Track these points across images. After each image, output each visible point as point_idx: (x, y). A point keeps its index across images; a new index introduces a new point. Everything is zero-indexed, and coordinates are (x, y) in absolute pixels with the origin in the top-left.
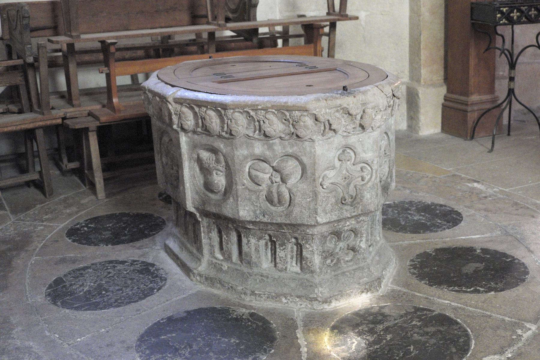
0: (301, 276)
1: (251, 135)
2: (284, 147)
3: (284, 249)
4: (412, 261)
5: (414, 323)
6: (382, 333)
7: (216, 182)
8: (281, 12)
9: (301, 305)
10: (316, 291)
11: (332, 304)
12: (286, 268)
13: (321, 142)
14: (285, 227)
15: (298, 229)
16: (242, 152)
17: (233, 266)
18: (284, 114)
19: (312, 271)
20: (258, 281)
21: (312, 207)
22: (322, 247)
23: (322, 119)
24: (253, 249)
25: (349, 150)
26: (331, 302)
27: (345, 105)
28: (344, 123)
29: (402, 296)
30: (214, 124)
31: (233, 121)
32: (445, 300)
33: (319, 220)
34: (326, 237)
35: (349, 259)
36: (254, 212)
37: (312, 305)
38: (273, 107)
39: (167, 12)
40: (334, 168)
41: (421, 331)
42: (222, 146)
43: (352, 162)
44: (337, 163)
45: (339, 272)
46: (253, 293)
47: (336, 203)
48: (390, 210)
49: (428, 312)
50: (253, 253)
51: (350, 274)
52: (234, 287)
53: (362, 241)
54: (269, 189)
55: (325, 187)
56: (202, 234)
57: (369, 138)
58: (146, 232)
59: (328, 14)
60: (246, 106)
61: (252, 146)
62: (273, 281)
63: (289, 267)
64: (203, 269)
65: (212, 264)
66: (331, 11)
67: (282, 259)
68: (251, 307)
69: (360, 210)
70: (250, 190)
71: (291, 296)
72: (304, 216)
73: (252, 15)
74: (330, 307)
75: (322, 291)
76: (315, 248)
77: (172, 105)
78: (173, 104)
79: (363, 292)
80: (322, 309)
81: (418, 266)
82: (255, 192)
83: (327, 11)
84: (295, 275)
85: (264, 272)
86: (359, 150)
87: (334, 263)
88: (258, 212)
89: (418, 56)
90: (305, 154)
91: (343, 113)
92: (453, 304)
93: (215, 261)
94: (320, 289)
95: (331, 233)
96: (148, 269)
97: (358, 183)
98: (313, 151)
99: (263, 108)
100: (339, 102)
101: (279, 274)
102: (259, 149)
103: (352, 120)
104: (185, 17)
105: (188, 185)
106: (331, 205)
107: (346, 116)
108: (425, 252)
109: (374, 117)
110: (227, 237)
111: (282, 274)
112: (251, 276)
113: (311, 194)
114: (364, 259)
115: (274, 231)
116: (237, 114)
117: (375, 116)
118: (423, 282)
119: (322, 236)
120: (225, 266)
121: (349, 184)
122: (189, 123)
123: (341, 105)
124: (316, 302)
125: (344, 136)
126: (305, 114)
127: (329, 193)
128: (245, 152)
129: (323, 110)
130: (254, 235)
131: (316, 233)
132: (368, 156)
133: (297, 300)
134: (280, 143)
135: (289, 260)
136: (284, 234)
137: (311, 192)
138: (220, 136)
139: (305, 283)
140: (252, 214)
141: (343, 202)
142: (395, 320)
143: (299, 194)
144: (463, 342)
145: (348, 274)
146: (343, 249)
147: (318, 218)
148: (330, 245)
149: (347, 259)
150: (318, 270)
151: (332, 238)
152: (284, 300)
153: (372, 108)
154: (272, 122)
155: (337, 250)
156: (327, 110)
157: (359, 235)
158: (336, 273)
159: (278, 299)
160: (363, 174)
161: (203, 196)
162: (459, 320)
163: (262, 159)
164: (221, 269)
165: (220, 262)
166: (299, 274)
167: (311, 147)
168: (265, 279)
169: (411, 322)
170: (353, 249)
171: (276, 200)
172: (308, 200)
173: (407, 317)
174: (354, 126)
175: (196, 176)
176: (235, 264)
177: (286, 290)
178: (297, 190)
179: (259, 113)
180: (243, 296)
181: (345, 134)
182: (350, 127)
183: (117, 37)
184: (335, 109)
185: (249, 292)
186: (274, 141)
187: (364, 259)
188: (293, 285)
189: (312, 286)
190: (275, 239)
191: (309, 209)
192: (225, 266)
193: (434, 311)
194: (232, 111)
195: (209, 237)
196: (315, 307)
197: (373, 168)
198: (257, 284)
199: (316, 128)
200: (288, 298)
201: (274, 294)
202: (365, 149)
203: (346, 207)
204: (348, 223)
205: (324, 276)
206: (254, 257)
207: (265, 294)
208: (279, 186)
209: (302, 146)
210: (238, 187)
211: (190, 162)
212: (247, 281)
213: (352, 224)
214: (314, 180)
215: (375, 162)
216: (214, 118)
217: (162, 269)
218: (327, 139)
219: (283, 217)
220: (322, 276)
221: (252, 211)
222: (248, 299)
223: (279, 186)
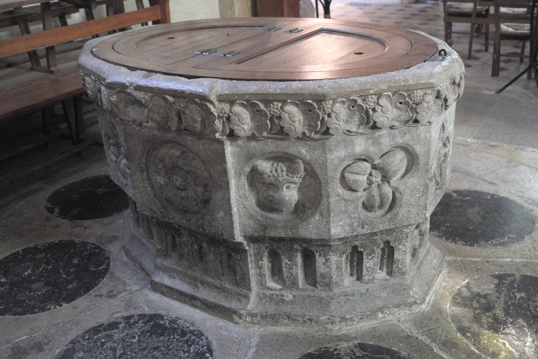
3: (372, 258)
7: (287, 198)
10: (411, 293)
17: (301, 293)
20: (343, 302)
24: (334, 267)
30: (297, 124)
31: (333, 115)
42: (304, 151)
46: (343, 319)
50: (333, 272)
52: (315, 318)
56: (250, 265)
61: (353, 144)
62: (361, 296)
64: (253, 306)
67: (369, 270)
70: (346, 200)
71: (388, 308)
75: (415, 292)
77: (214, 106)
78: (216, 103)
82: (353, 201)
89: (231, 8)
90: (419, 141)
93: (268, 293)
96: (159, 325)
98: (428, 136)
101: (367, 287)
110: (289, 261)
111: (369, 286)
112: (333, 299)
122: (246, 127)
128: (342, 153)
137: (421, 186)
138: (303, 138)
139: (398, 288)
143: (408, 191)
152: (380, 315)
159: (373, 316)
161: (262, 219)
163: (363, 157)
164: (283, 301)
165: (278, 293)
167: (426, 131)
168: (351, 298)
172: (418, 195)
176: (303, 290)
177: (379, 303)
179: (370, 100)
180: (329, 326)
185: (337, 320)
186: (381, 133)
188: (384, 295)
189: (406, 288)
190: (362, 250)
191: (418, 206)
192: (288, 296)
195: (257, 268)
198: (343, 306)
201: (368, 313)
206: (334, 277)
210: (330, 200)
212: (328, 306)
219: (387, 223)
222: (336, 328)
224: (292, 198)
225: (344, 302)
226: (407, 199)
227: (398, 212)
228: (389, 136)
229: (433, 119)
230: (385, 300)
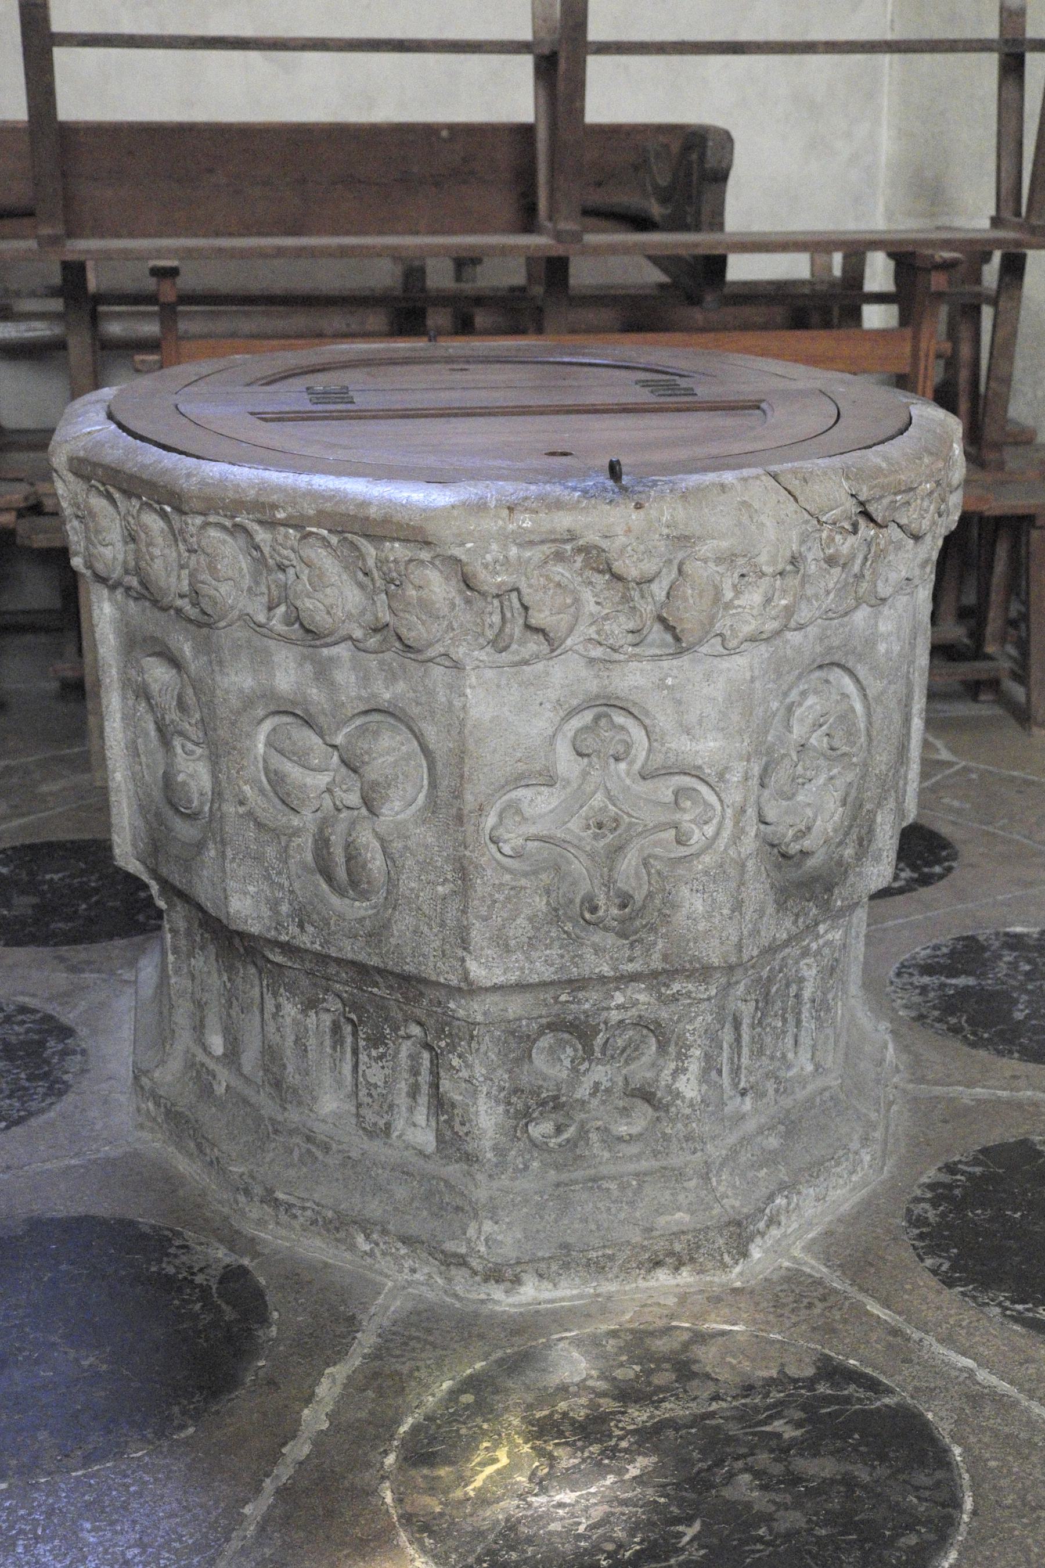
0: (430, 1167)
1: (261, 618)
2: (365, 679)
3: (381, 1057)
4: (951, 1169)
5: (777, 1426)
6: (624, 1444)
7: (181, 778)
8: (890, 216)
9: (413, 1271)
10: (471, 1232)
11: (522, 1290)
12: (388, 1126)
13: (489, 674)
14: (380, 980)
15: (422, 994)
16: (238, 680)
18: (358, 549)
19: (467, 1154)
20: (296, 1154)
21: (451, 915)
22: (510, 1071)
23: (493, 580)
25: (620, 719)
26: (517, 1281)
27: (592, 537)
28: (593, 608)
29: (810, 1306)
32: (964, 1354)
33: (476, 971)
34: (528, 1041)
35: (635, 1130)
36: (274, 905)
37: (449, 1280)
38: (322, 518)
39: (437, 184)
40: (550, 780)
41: (777, 1469)
43: (637, 766)
44: (566, 763)
45: (579, 1174)
46: (269, 1199)
47: (555, 915)
48: (1008, 957)
49: (861, 1394)
50: (288, 1053)
51: (623, 1187)
53: (685, 1070)
54: (321, 830)
55: (507, 849)
57: (708, 677)
58: (141, 918)
59: (996, 222)
60: (239, 505)
62: (343, 1165)
63: (399, 1124)
64: (169, 1078)
65: (193, 1065)
66: (1007, 215)
67: (374, 1092)
68: (251, 1246)
69: (656, 956)
70: (259, 825)
71: (384, 1232)
72: (426, 950)
73: (706, 209)
74: (510, 1300)
75: (494, 1236)
76: (480, 1071)
78: (70, 477)
79: (658, 1264)
80: (482, 1301)
81: (957, 1192)
82: (276, 833)
83: (993, 213)
84: (414, 1159)
85: (319, 1128)
86: (664, 719)
87: (566, 1136)
88: (284, 908)
90: (432, 713)
91: (587, 564)
92: (983, 1376)
93: (201, 1057)
94: (488, 1226)
95: (552, 1027)
97: (658, 851)
98: (457, 703)
99: (290, 517)
100: (564, 521)
102: (287, 674)
103: (626, 599)
104: (502, 203)
105: (118, 776)
106: (530, 919)
107: (600, 580)
108: (1024, 1144)
109: (729, 595)
110: (230, 980)
111: (375, 1147)
113: (448, 868)
114: (688, 1138)
115: (346, 983)
116: (214, 533)
117: (738, 592)
118: (929, 1262)
119: (512, 1033)
120: (223, 1080)
121: (617, 850)
122: (108, 552)
123: (571, 536)
124: (464, 1272)
125: (591, 661)
126: (425, 555)
127: (525, 874)
129: (494, 547)
130: (292, 988)
131: (479, 1018)
132: (707, 748)
133: (403, 1251)
134: (353, 658)
135: (402, 1100)
136: (381, 1006)
140: (266, 913)
141: (587, 916)
142: (716, 1398)
144: (911, 1550)
145: (613, 1186)
146: (607, 1091)
147: (472, 966)
148: (551, 1065)
149: (623, 1129)
150: (489, 1155)
151: (562, 1044)
153: (719, 560)
154: (321, 576)
155: (583, 1091)
156: (514, 551)
157: (672, 1049)
158: (565, 1177)
159: (341, 1235)
160: (677, 816)
162: (957, 1450)
166: (427, 1157)
168: (319, 1154)
169: (770, 1419)
170: (647, 1096)
171: (341, 873)
172: (440, 888)
173: (767, 1395)
174: (631, 626)
175: (141, 748)
176: (247, 1080)
177: (374, 1208)
178: (406, 847)
180: (242, 1198)
181: (597, 652)
182: (618, 628)
183: (189, 254)
184: (547, 549)
185: (258, 1190)
186: (334, 651)
187: (688, 1138)
188: (401, 1193)
189: (464, 1210)
191: (443, 925)
193: (889, 1391)
194: (199, 520)
196: (459, 1289)
197: (728, 801)
198: (293, 1165)
199: (465, 617)
200: (375, 1236)
201: (330, 1214)
202: (692, 718)
203: (597, 937)
204: (619, 998)
205: (512, 1179)
206: (290, 1069)
207: (304, 1209)
208: (353, 824)
209: (422, 678)
211: (124, 698)
213: (635, 1003)
214: (460, 819)
215: (735, 777)
216: (160, 540)
217: (84, 1052)
218: (515, 664)
219: (361, 942)
220: (505, 1181)
221: (268, 900)
222: (254, 1212)
223: (353, 824)
224: (192, 784)
225: (301, 1155)
226: (412, 890)
227: (389, 920)
228: (354, 669)
229: (462, 650)
230: (396, 1209)
